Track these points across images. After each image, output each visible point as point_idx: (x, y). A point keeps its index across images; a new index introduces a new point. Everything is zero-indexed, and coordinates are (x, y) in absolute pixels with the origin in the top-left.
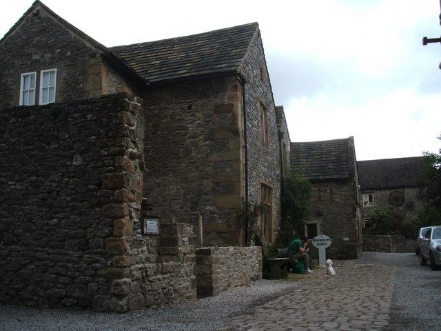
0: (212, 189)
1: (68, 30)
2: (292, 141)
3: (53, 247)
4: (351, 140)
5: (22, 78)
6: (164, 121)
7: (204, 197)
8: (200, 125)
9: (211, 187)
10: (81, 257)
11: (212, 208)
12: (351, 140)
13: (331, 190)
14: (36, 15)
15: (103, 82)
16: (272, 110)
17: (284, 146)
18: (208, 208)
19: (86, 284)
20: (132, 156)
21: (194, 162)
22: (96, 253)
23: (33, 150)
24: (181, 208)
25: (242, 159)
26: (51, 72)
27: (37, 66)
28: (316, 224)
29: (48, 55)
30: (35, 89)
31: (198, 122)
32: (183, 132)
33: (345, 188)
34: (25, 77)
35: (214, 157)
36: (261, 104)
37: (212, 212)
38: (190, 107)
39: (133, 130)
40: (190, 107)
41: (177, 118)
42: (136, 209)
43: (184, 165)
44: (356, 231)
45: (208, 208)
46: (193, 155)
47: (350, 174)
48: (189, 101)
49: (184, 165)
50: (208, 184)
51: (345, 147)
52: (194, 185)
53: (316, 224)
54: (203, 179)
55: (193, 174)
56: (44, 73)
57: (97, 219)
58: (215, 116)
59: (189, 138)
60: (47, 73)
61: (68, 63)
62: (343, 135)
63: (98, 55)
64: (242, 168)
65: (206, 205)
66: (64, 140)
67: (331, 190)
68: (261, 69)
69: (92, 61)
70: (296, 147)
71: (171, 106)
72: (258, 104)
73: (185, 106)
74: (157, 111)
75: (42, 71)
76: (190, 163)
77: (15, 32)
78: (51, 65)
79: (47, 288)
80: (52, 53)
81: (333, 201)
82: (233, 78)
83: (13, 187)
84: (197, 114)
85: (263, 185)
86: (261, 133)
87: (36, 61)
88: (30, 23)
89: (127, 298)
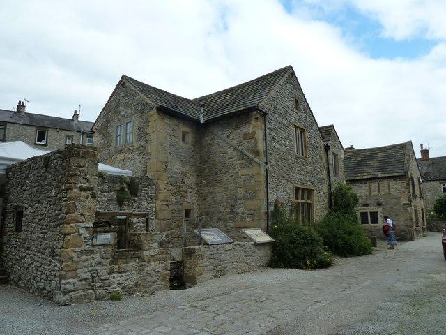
14: (122, 85)
17: (335, 155)
20: (83, 189)
35: (244, 172)
43: (226, 178)
49: (226, 178)
50: (241, 192)
64: (263, 179)
68: (297, 101)
69: (151, 112)
85: (297, 189)
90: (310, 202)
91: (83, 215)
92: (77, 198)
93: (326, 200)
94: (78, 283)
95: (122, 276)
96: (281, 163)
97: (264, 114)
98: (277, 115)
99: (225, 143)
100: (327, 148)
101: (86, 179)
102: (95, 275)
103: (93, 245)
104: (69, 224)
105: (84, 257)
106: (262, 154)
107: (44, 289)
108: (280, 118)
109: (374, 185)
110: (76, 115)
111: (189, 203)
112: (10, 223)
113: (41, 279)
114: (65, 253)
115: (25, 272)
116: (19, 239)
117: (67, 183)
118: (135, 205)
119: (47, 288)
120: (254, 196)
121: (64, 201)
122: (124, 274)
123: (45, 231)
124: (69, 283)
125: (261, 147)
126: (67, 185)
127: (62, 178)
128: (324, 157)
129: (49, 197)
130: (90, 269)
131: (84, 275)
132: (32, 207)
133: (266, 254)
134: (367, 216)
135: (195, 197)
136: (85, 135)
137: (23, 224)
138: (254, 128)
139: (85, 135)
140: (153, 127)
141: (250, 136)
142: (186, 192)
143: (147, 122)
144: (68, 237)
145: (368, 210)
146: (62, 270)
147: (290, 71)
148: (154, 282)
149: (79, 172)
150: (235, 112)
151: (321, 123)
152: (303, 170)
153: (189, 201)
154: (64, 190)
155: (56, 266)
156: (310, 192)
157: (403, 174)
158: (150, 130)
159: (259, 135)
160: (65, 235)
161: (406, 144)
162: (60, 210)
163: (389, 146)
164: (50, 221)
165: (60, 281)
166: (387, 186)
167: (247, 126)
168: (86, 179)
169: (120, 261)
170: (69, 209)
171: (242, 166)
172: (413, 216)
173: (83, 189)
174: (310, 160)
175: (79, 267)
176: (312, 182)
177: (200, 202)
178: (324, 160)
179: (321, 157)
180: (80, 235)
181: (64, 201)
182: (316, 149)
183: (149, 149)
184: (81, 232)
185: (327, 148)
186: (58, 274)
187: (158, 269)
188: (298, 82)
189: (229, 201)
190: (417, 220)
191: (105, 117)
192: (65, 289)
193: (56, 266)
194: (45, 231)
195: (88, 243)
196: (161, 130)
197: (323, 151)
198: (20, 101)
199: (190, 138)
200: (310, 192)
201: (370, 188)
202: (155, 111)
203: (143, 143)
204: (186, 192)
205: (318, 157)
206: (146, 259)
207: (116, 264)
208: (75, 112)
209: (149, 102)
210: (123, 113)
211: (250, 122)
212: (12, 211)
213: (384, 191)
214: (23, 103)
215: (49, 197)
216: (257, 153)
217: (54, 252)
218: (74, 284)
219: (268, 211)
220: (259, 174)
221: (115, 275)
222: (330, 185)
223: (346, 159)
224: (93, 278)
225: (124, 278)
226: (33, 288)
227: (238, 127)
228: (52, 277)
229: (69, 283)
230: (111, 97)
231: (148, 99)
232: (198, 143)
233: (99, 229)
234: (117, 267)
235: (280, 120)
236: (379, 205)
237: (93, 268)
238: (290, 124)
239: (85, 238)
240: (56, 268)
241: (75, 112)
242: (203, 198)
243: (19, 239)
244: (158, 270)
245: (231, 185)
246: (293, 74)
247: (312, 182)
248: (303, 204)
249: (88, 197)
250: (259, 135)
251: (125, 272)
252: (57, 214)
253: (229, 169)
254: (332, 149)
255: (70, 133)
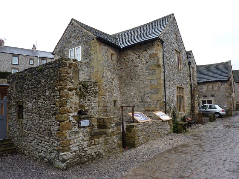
0: (149, 92)
1: (84, 29)
2: (198, 64)
3: (41, 133)
4: (230, 62)
5: (76, 49)
6: (129, 63)
7: (146, 95)
8: (144, 64)
9: (149, 91)
10: (49, 140)
11: (149, 100)
12: (230, 62)
13: (219, 85)
14: (72, 25)
15: (98, 50)
16: (184, 53)
17: (193, 68)
18: (148, 100)
19: (51, 152)
20: (70, 90)
21: (142, 80)
22: (54, 138)
23: (34, 88)
24: (138, 100)
25: (162, 78)
26: (79, 48)
27: (74, 46)
28: (211, 100)
29: (77, 41)
30: (74, 55)
31: (143, 63)
32: (137, 67)
33: (225, 84)
34: (70, 51)
35: (150, 78)
36: (176, 51)
37: (150, 102)
38: (139, 56)
39: (70, 76)
40: (139, 56)
41: (134, 61)
42: (74, 116)
43: (138, 82)
44: (231, 104)
45: (148, 100)
46: (141, 77)
47: (228, 78)
48: (139, 54)
49: (138, 82)
50: (148, 90)
51: (227, 65)
52: (142, 90)
53: (211, 100)
54: (146, 87)
55: (142, 85)
56: (77, 48)
57: (54, 121)
58: (150, 59)
59: (140, 70)
60: (78, 48)
61: (85, 43)
62: (226, 60)
63: (95, 38)
64: (162, 82)
65: (147, 99)
66: (43, 83)
67: (219, 85)
68: (176, 35)
69: (93, 41)
70: (202, 68)
71: (132, 57)
72: (174, 51)
73: (137, 56)
74: (126, 60)
75: (76, 48)
76: (141, 80)
77: (66, 33)
78: (78, 45)
79: (39, 152)
80: (79, 40)
81: (219, 90)
82: (157, 41)
83: (28, 105)
84: (142, 59)
85: (177, 87)
86: (176, 64)
87: (74, 44)
88: (71, 28)
89: (67, 162)
90: (183, 95)
91: (71, 108)
92: (67, 96)
93: (190, 94)
94: (71, 154)
95: (96, 147)
96: (170, 72)
97: (162, 42)
98: (168, 43)
99: (140, 61)
100: (190, 64)
101: (72, 83)
102: (81, 148)
103: (79, 127)
104: (62, 114)
105: (73, 137)
106: (162, 67)
107: (45, 158)
108: (169, 45)
109: (210, 85)
110: (34, 47)
111: (115, 97)
112: (13, 113)
113: (42, 151)
114: (61, 134)
115: (28, 145)
116: (21, 123)
117: (59, 85)
118: (87, 98)
119: (48, 157)
120: (157, 92)
121: (58, 98)
122: (97, 146)
123: (43, 119)
124: (65, 155)
125: (161, 62)
126: (59, 87)
127: (54, 82)
128: (188, 69)
129: (44, 95)
130: (77, 144)
131: (75, 149)
132: (31, 102)
133: (168, 128)
134: (208, 102)
135: (119, 93)
136: (40, 59)
137: (24, 114)
138: (156, 50)
139: (40, 59)
140: (94, 50)
141: (156, 55)
142: (114, 90)
143: (90, 47)
144: (63, 123)
145: (206, 99)
146: (59, 146)
147: (173, 17)
148: (114, 148)
149: (67, 78)
150: (130, 45)
151: (187, 50)
152: (180, 76)
153: (115, 95)
154: (56, 90)
155: (54, 142)
156: (183, 88)
157: (227, 79)
158: (92, 52)
159: (160, 55)
160: (60, 121)
161: (227, 62)
162: (55, 104)
163: (211, 65)
164: (46, 112)
165: (59, 153)
166: (217, 86)
167: (152, 49)
168: (72, 83)
169: (95, 137)
170: (63, 104)
171: (149, 74)
172: (232, 103)
173: (70, 90)
174: (183, 71)
175: (71, 143)
176: (184, 84)
177: (121, 96)
178: (188, 71)
179: (187, 70)
180: (70, 121)
181: (58, 98)
182: (185, 64)
183: (93, 64)
184: (71, 119)
185: (190, 64)
186: (56, 148)
187: (116, 140)
188: (177, 24)
189: (140, 95)
190: (233, 105)
191: (61, 45)
192: (63, 159)
193: (54, 142)
194: (43, 119)
195: (76, 127)
196: (102, 54)
197: (188, 66)
198: (1, 39)
199: (115, 57)
200: (183, 88)
201: (208, 87)
202: (95, 40)
203: (88, 60)
204: (114, 90)
205: (186, 69)
206: (109, 135)
207: (93, 140)
208: (34, 45)
209: (91, 34)
210: (73, 42)
211: (153, 47)
212: (15, 105)
213: (216, 88)
214: (3, 40)
215: (44, 95)
216: (159, 66)
217: (51, 133)
218: (69, 155)
219: (165, 101)
220: (160, 79)
221: (93, 147)
222: (191, 86)
223: (198, 70)
224: (80, 150)
225: (98, 148)
226: (36, 156)
227: (145, 50)
228: (52, 150)
229: (65, 155)
230: (65, 32)
231: (90, 33)
232: (119, 61)
233: (83, 116)
234: (93, 141)
235: (169, 46)
236: (213, 96)
237: (79, 144)
238: (174, 49)
239: (73, 123)
240: (54, 144)
241: (34, 45)
242: (123, 93)
243: (21, 123)
244: (116, 141)
245: (142, 86)
246: (174, 19)
247: (184, 84)
248: (180, 96)
249: (73, 95)
250: (160, 55)
251: (98, 144)
252: (52, 107)
253: (139, 76)
254: (192, 65)
255: (32, 58)
